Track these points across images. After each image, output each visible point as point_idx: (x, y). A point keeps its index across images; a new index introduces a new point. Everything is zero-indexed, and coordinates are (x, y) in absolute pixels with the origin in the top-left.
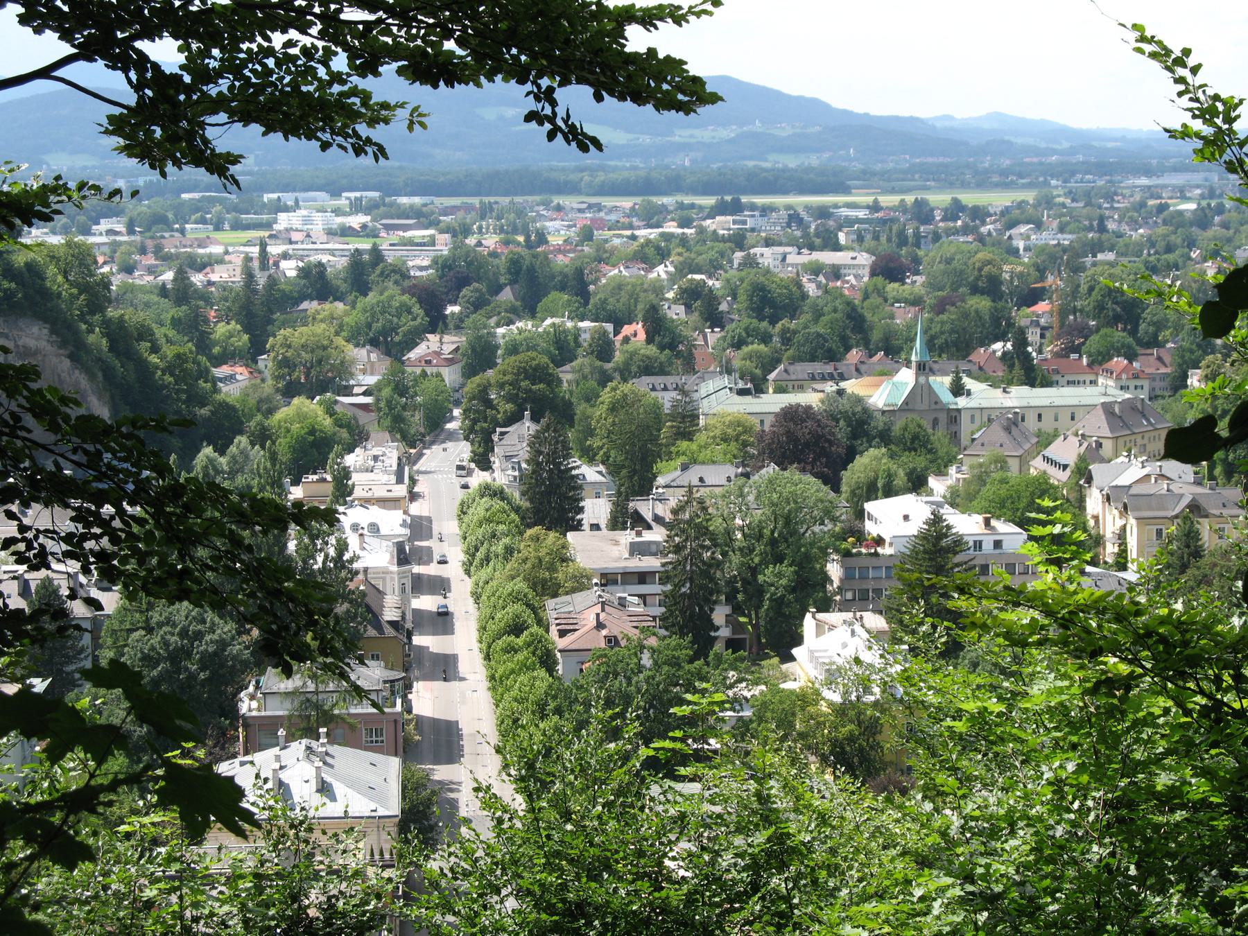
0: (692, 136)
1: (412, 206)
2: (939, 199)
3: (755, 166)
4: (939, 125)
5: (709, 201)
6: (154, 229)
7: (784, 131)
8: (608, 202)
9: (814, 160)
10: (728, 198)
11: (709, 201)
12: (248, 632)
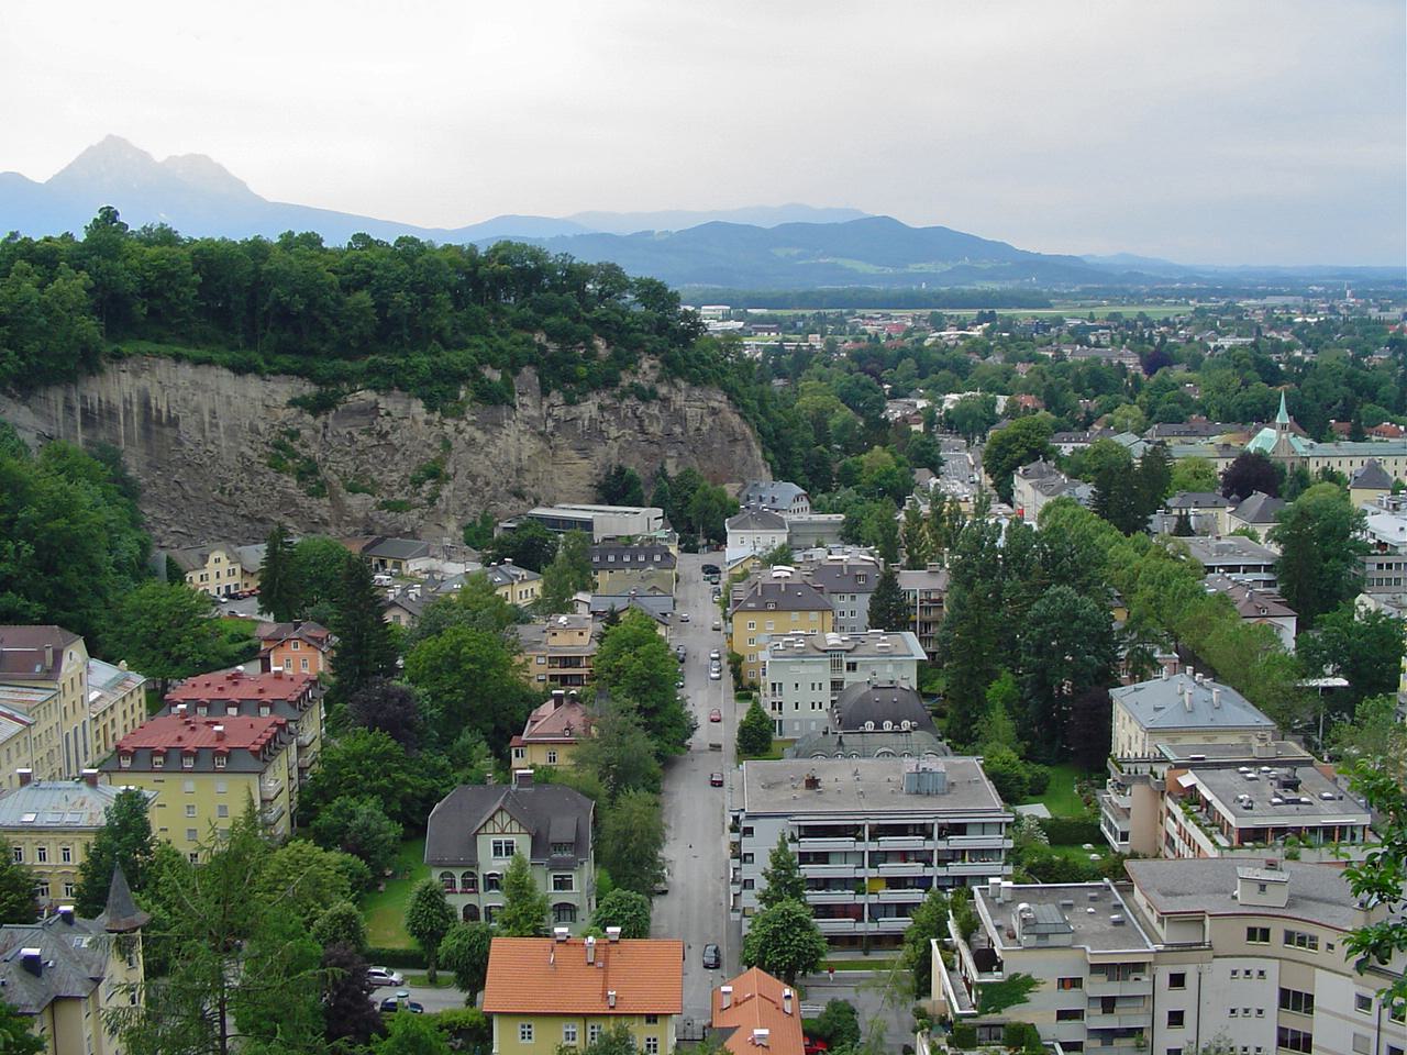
0: (921, 268)
1: (762, 316)
2: (1103, 311)
3: (970, 290)
4: (1089, 261)
5: (974, 313)
6: (37, 267)
7: (985, 265)
8: (894, 313)
9: (1009, 286)
10: (987, 311)
11: (974, 313)
12: (1103, 541)
